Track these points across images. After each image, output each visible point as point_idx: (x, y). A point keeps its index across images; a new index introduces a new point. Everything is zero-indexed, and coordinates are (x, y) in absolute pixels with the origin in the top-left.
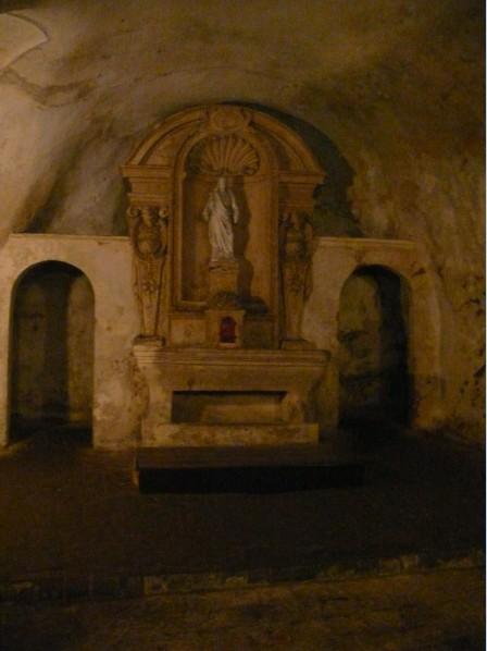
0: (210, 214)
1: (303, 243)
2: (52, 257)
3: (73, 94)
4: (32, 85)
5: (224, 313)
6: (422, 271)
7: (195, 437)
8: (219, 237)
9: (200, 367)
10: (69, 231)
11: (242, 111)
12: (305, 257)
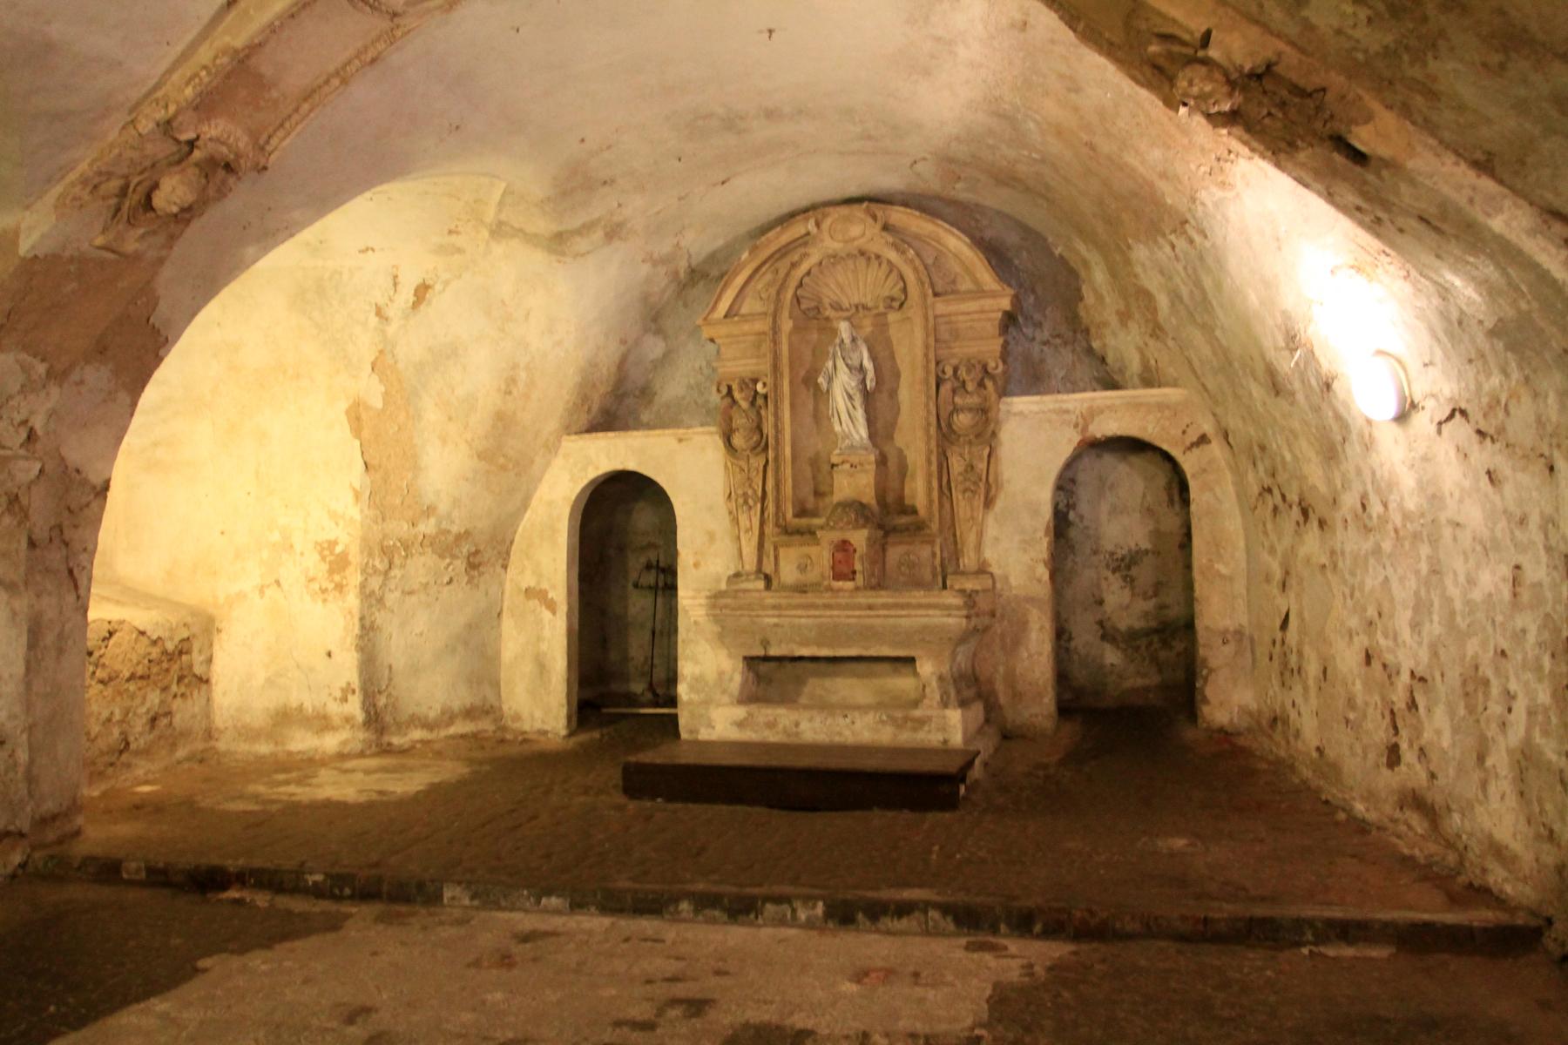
0: (830, 381)
1: (983, 411)
2: (618, 466)
3: (598, 235)
4: (536, 235)
5: (836, 536)
6: (1203, 439)
7: (771, 725)
8: (844, 417)
9: (775, 620)
10: (664, 422)
11: (868, 211)
12: (986, 432)
